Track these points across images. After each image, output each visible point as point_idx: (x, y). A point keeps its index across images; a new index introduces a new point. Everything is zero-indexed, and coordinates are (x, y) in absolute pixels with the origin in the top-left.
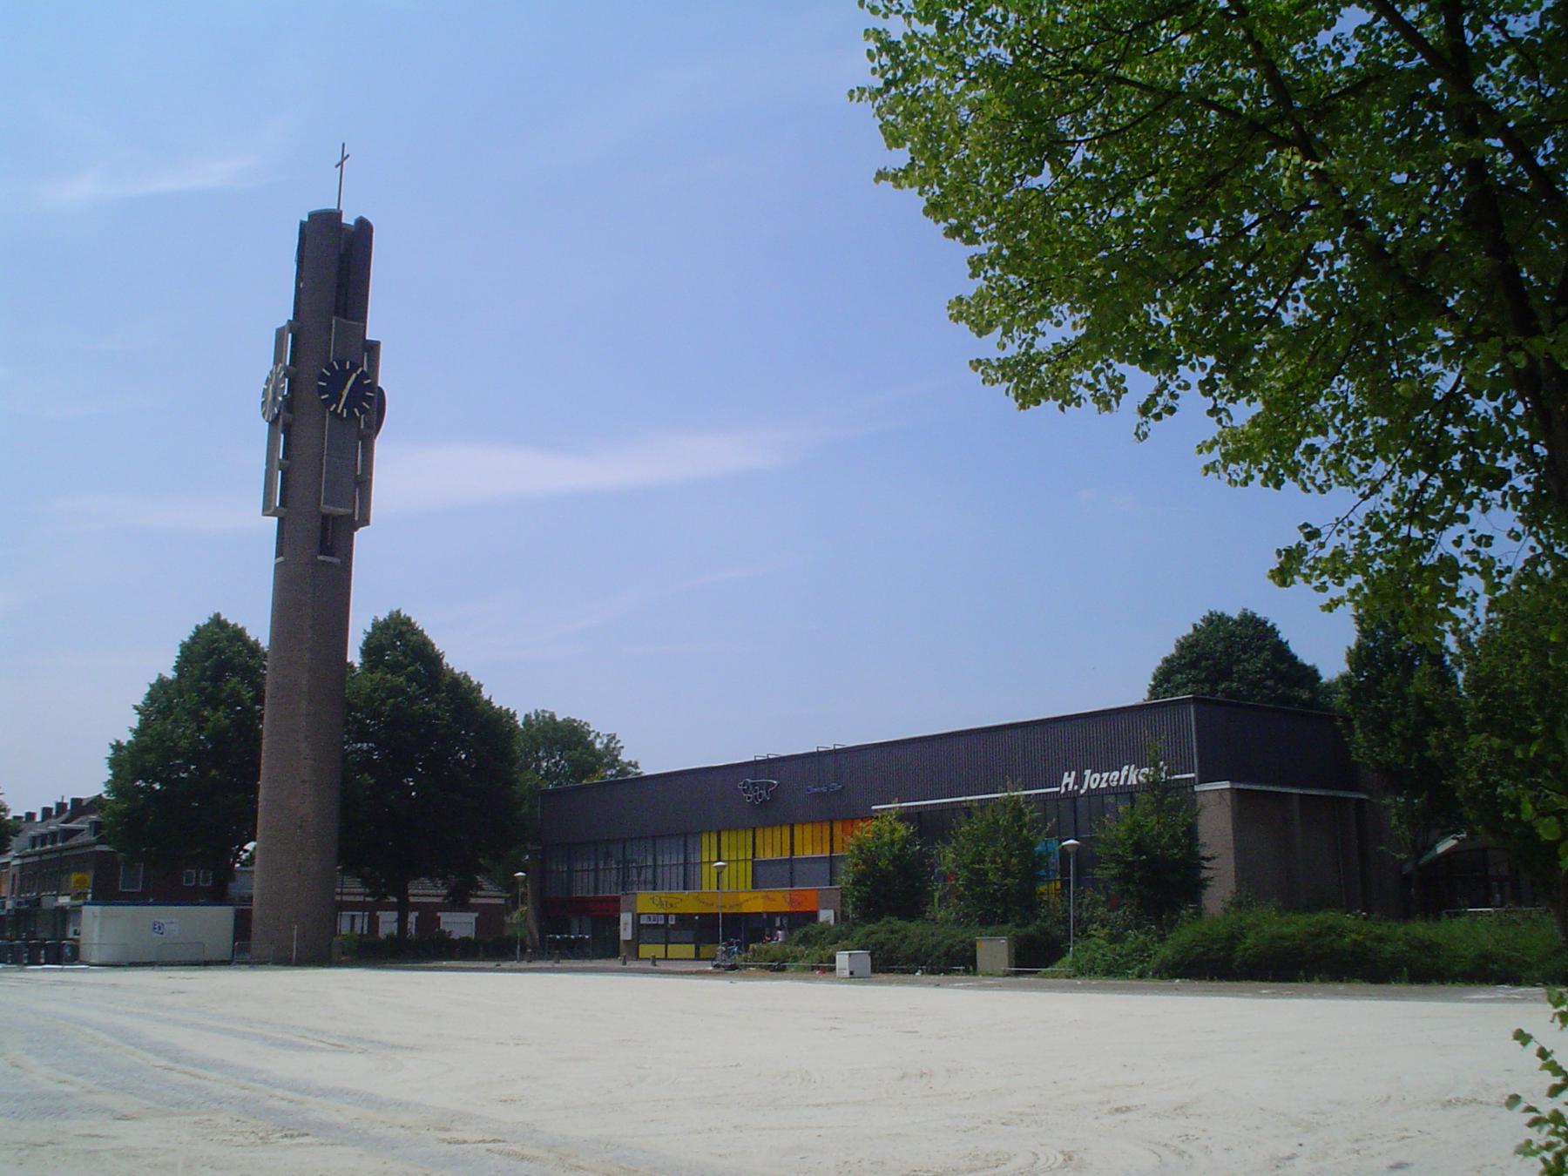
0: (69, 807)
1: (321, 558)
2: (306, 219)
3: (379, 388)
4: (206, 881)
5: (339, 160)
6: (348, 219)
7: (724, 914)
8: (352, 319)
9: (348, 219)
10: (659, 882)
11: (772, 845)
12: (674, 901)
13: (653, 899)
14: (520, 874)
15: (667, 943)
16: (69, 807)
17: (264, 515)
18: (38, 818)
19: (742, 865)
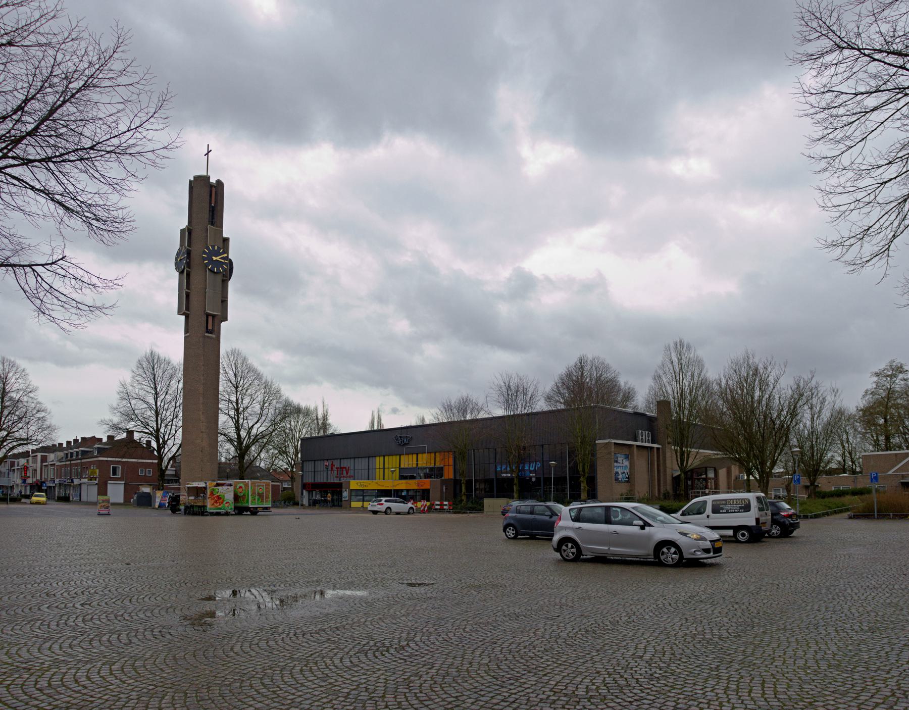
0: (80, 441)
1: (207, 334)
2: (193, 179)
3: (230, 259)
4: (149, 473)
5: (207, 152)
6: (213, 180)
7: (394, 490)
8: (873, 505)
9: (213, 180)
10: (370, 477)
11: (408, 461)
12: (366, 484)
13: (357, 483)
14: (553, 462)
15: (363, 501)
16: (80, 441)
17: (178, 314)
18: (65, 445)
19: (307, 470)
